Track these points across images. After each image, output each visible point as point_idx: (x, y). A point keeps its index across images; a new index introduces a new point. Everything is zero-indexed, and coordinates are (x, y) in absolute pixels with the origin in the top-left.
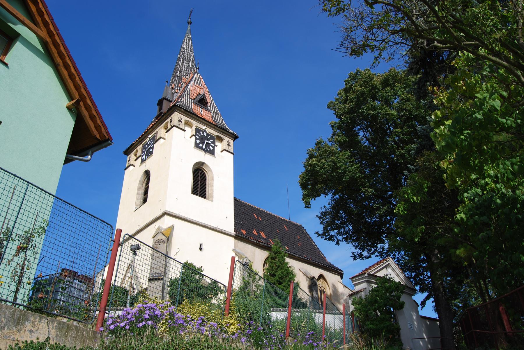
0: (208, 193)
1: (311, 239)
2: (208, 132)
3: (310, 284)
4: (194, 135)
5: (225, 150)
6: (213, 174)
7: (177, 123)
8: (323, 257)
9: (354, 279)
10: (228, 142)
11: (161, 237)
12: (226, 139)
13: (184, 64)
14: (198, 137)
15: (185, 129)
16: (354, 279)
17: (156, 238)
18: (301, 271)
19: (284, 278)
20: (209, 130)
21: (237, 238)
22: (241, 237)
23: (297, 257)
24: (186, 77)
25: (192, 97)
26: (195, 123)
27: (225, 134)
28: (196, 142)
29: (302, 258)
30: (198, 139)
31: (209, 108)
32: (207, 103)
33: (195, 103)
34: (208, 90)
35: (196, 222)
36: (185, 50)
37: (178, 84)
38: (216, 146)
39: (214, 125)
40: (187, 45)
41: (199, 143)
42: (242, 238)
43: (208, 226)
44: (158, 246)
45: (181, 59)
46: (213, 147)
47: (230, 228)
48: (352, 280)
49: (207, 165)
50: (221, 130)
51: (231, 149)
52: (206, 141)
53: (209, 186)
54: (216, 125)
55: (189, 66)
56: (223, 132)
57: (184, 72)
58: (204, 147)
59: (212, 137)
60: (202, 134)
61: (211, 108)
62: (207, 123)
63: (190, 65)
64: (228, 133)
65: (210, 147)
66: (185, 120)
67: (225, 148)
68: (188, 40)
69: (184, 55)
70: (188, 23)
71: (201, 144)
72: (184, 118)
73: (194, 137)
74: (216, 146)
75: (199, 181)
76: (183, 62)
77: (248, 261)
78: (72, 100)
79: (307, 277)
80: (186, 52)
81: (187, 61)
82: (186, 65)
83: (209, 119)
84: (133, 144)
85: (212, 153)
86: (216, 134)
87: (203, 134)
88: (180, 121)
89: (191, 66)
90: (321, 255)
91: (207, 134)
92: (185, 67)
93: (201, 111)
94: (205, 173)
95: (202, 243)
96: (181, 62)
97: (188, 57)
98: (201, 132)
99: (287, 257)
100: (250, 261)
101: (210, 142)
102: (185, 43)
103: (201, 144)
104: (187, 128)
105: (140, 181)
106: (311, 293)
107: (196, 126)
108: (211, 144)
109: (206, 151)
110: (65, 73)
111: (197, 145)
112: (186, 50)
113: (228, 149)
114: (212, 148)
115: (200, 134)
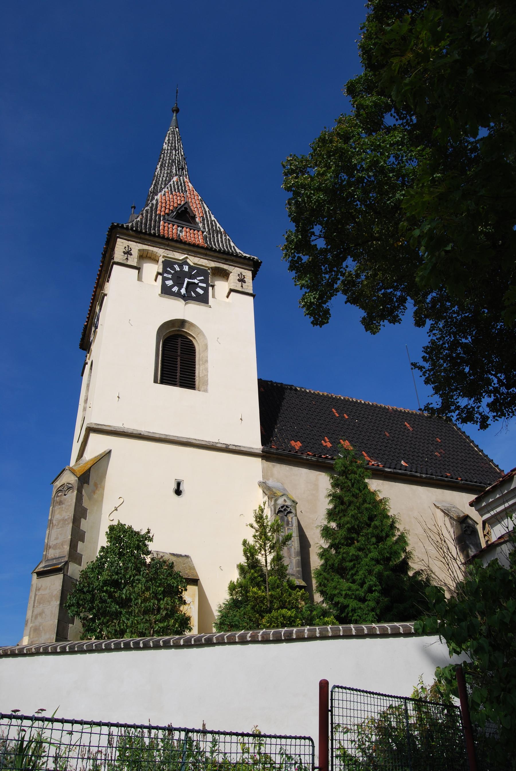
0: (199, 377)
1: (469, 440)
2: (192, 264)
3: (460, 532)
5: (231, 290)
6: (206, 339)
7: (121, 257)
8: (496, 472)
9: (484, 504)
12: (235, 272)
14: (170, 276)
16: (484, 504)
18: (438, 507)
19: (362, 528)
20: (192, 260)
21: (270, 457)
22: (276, 454)
23: (425, 478)
26: (161, 252)
27: (232, 261)
29: (437, 480)
30: (168, 279)
31: (201, 225)
32: (194, 217)
34: (200, 198)
35: (163, 437)
36: (166, 152)
39: (202, 248)
41: (172, 286)
42: (281, 455)
43: (194, 441)
44: (62, 499)
48: (479, 507)
49: (192, 325)
50: (220, 255)
51: (249, 286)
52: (186, 280)
53: (201, 362)
54: (207, 249)
56: (226, 260)
58: (183, 291)
59: (201, 271)
61: (204, 224)
62: (187, 247)
64: (238, 260)
65: (199, 290)
66: (139, 250)
67: (232, 288)
68: (171, 136)
69: (163, 159)
70: (173, 112)
71: (176, 287)
72: (136, 247)
73: (160, 278)
75: (179, 358)
76: (161, 170)
77: (288, 503)
79: (451, 518)
80: (167, 152)
82: (166, 172)
83: (200, 241)
84: (86, 326)
85: (203, 299)
86: (213, 264)
90: (492, 467)
91: (190, 267)
92: (163, 176)
94: (191, 341)
95: (179, 478)
97: (170, 159)
99: (369, 478)
100: (293, 501)
101: (196, 281)
103: (176, 287)
106: (465, 552)
107: (164, 257)
108: (200, 284)
109: (186, 298)
111: (166, 291)
112: (168, 149)
113: (240, 289)
115: (174, 269)
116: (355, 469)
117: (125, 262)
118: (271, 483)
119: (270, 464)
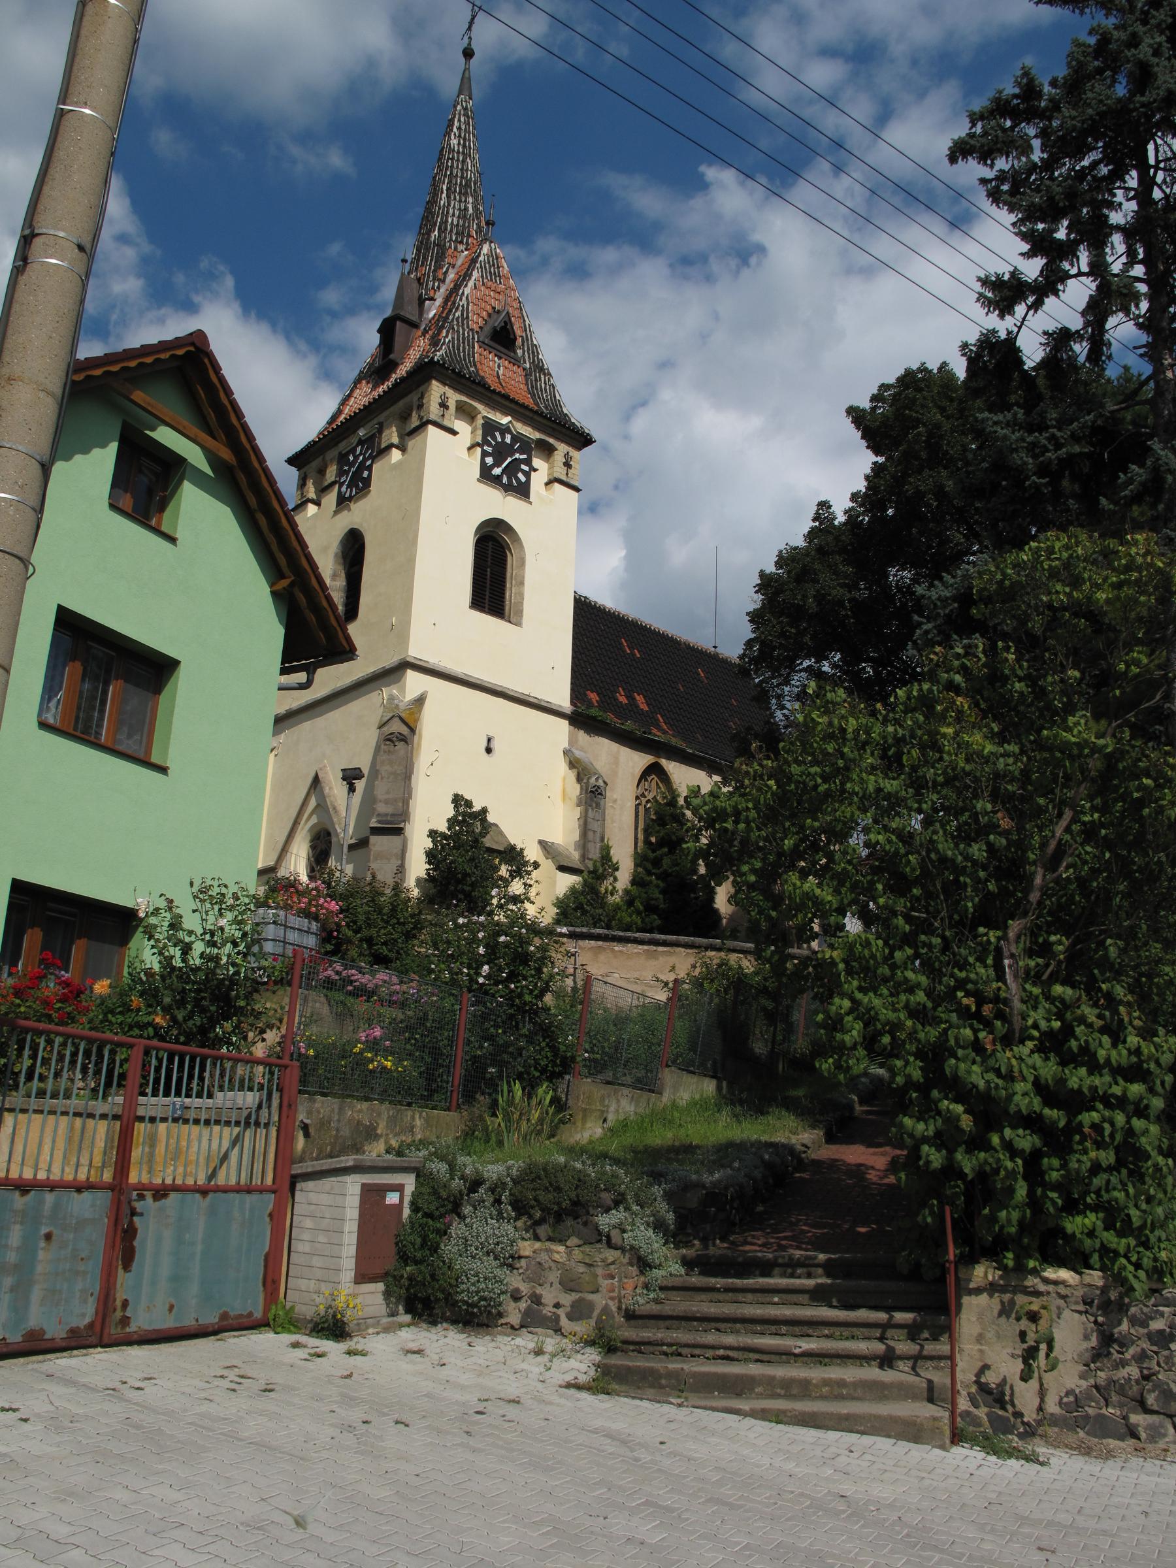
4: (478, 444)
10: (567, 455)
11: (397, 727)
13: (452, 203)
14: (489, 450)
15: (456, 428)
17: (387, 730)
24: (456, 249)
25: (475, 321)
26: (484, 411)
28: (483, 463)
30: (488, 454)
31: (519, 352)
33: (482, 344)
37: (435, 271)
38: (535, 470)
39: (531, 410)
40: (460, 136)
45: (445, 187)
46: (527, 475)
47: (560, 694)
54: (536, 412)
55: (466, 209)
57: (451, 231)
59: (526, 446)
60: (499, 439)
63: (470, 206)
65: (520, 476)
67: (557, 475)
69: (452, 173)
72: (454, 397)
73: (479, 450)
74: (535, 470)
76: (448, 197)
77: (600, 783)
78: (282, 576)
81: (460, 193)
82: (457, 206)
85: (523, 491)
87: (503, 437)
88: (443, 405)
89: (471, 211)
92: (453, 215)
93: (499, 367)
96: (444, 195)
97: (462, 177)
98: (497, 434)
102: (455, 130)
104: (460, 425)
105: (336, 555)
109: (508, 489)
110: (262, 521)
111: (486, 475)
112: (458, 152)
113: (564, 478)
114: (523, 479)
115: (494, 438)
116: (1165, 1048)
117: (439, 420)
118: (578, 753)
119: (581, 735)
